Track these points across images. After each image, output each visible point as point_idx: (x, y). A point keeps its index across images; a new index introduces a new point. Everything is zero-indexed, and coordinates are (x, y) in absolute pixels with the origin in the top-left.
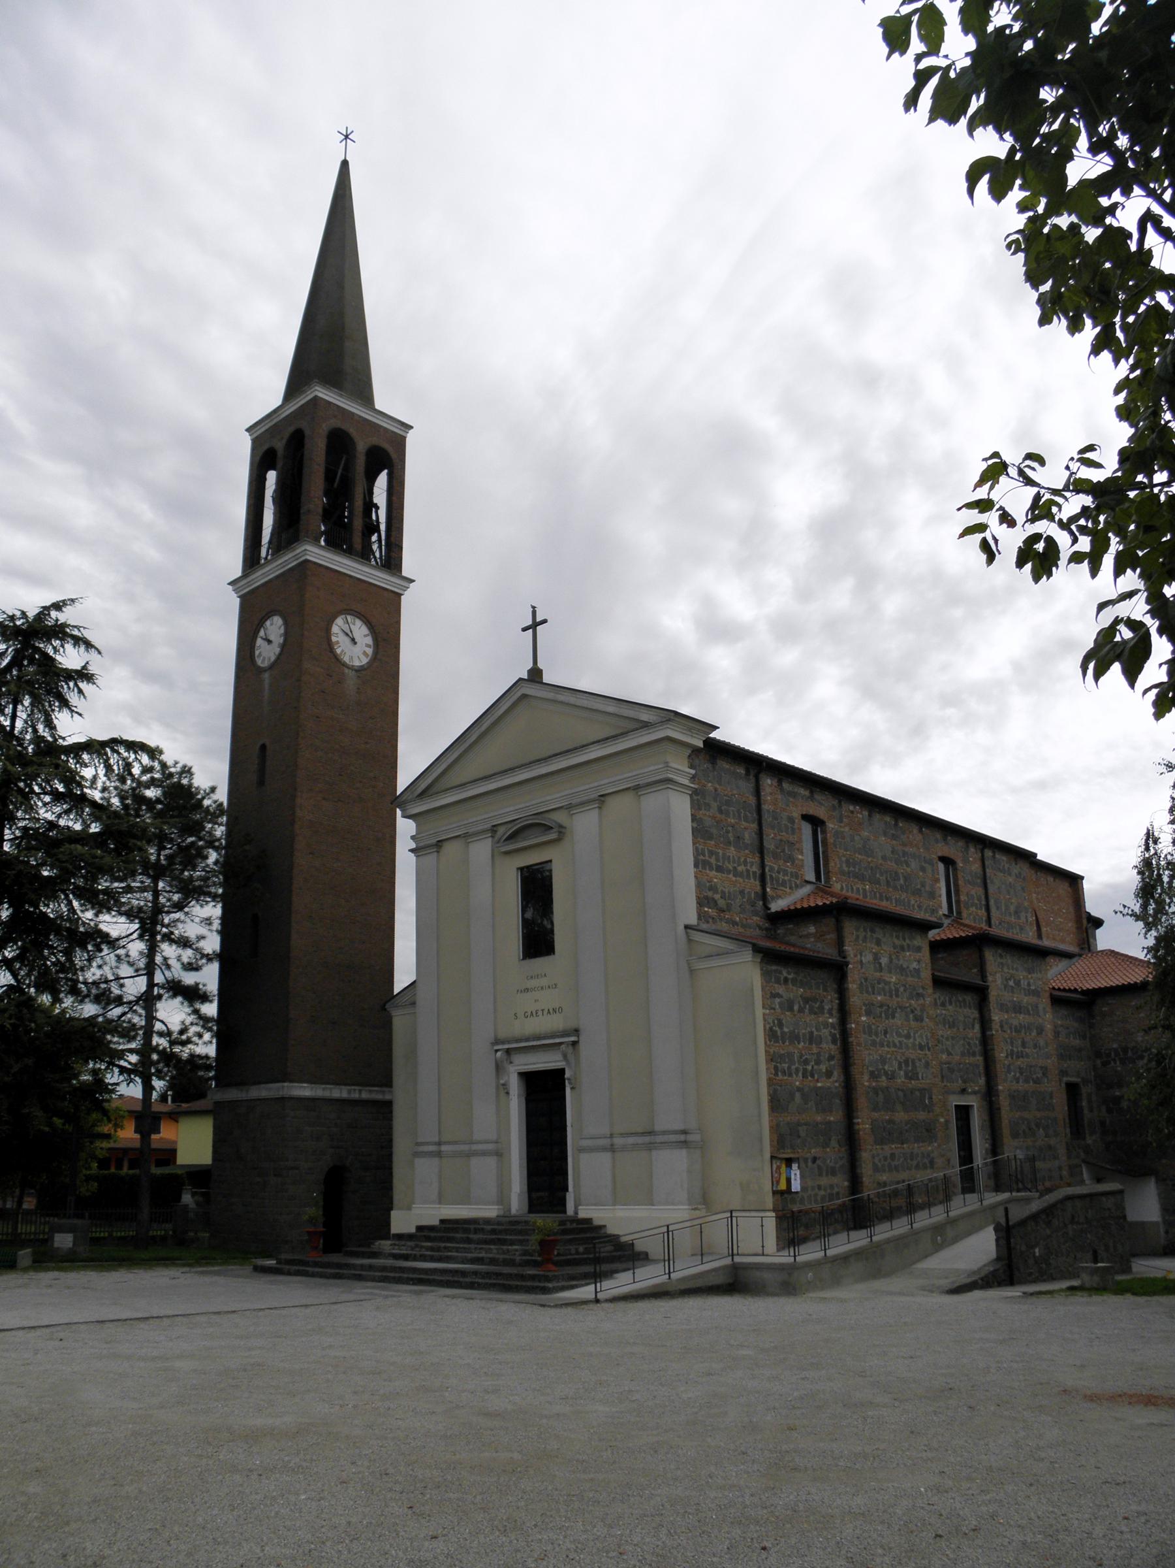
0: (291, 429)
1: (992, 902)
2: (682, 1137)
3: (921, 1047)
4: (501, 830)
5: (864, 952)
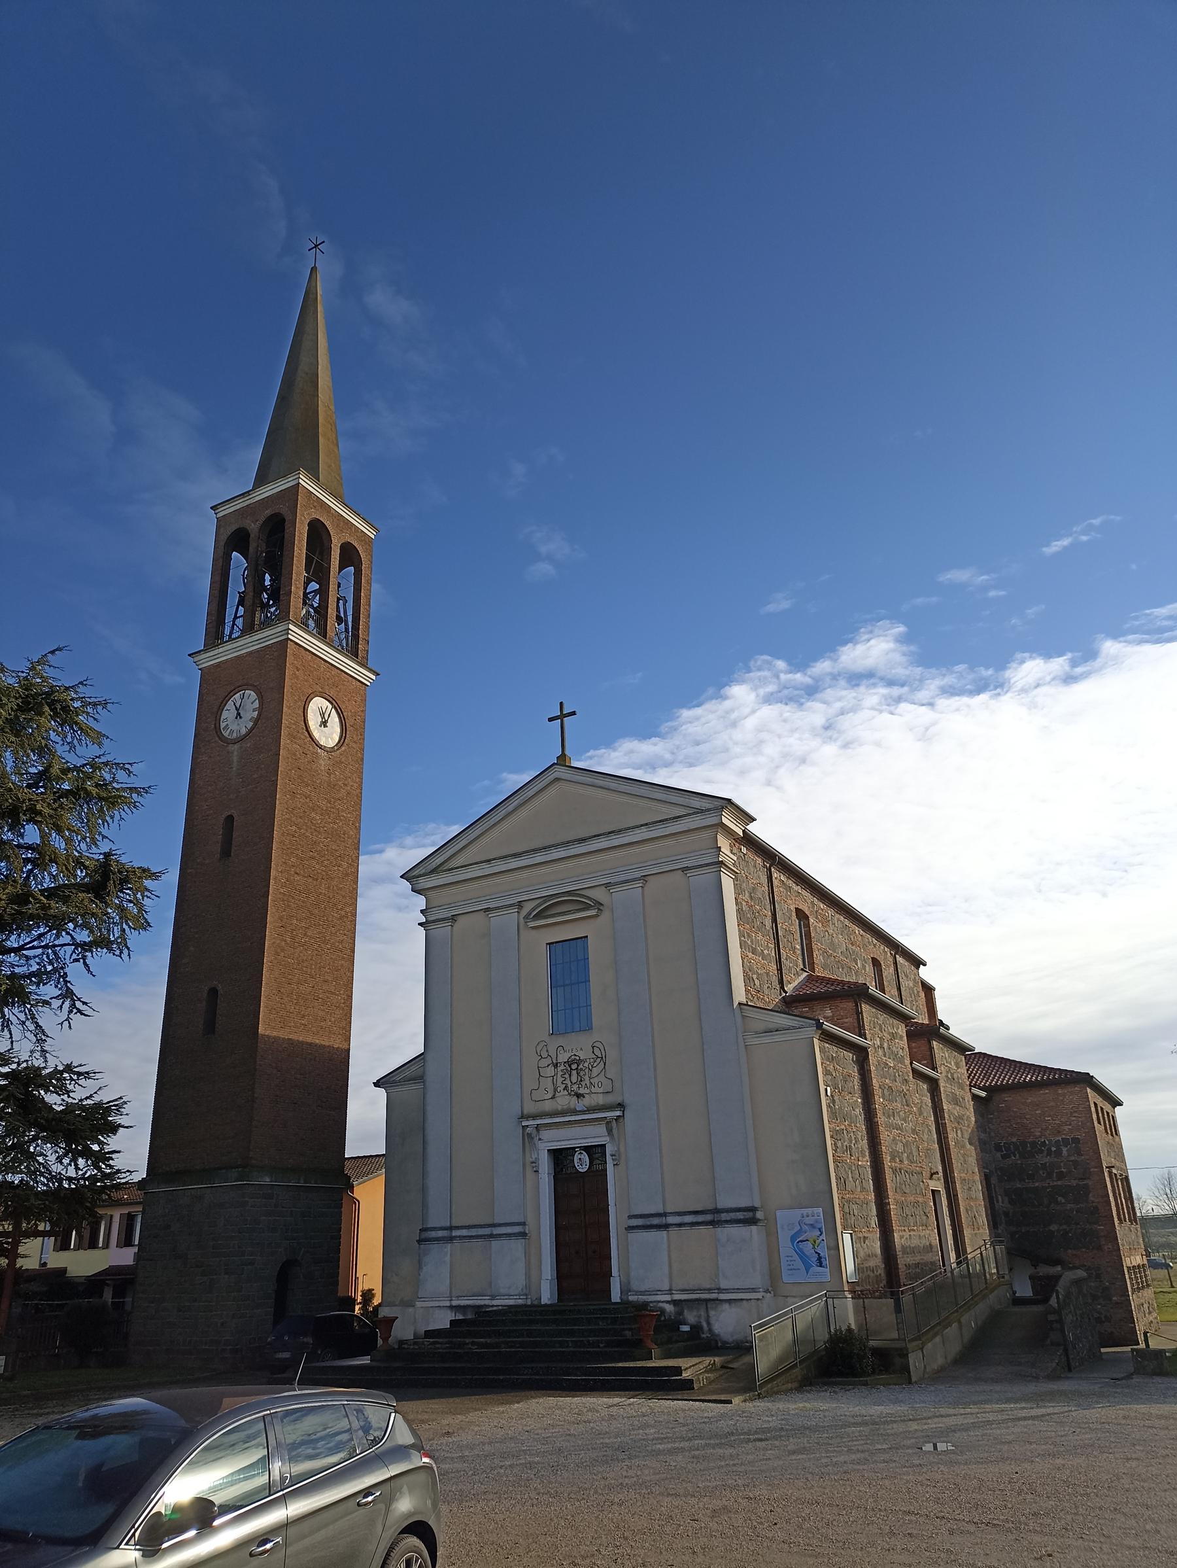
0: (268, 512)
2: (750, 1214)
4: (528, 907)
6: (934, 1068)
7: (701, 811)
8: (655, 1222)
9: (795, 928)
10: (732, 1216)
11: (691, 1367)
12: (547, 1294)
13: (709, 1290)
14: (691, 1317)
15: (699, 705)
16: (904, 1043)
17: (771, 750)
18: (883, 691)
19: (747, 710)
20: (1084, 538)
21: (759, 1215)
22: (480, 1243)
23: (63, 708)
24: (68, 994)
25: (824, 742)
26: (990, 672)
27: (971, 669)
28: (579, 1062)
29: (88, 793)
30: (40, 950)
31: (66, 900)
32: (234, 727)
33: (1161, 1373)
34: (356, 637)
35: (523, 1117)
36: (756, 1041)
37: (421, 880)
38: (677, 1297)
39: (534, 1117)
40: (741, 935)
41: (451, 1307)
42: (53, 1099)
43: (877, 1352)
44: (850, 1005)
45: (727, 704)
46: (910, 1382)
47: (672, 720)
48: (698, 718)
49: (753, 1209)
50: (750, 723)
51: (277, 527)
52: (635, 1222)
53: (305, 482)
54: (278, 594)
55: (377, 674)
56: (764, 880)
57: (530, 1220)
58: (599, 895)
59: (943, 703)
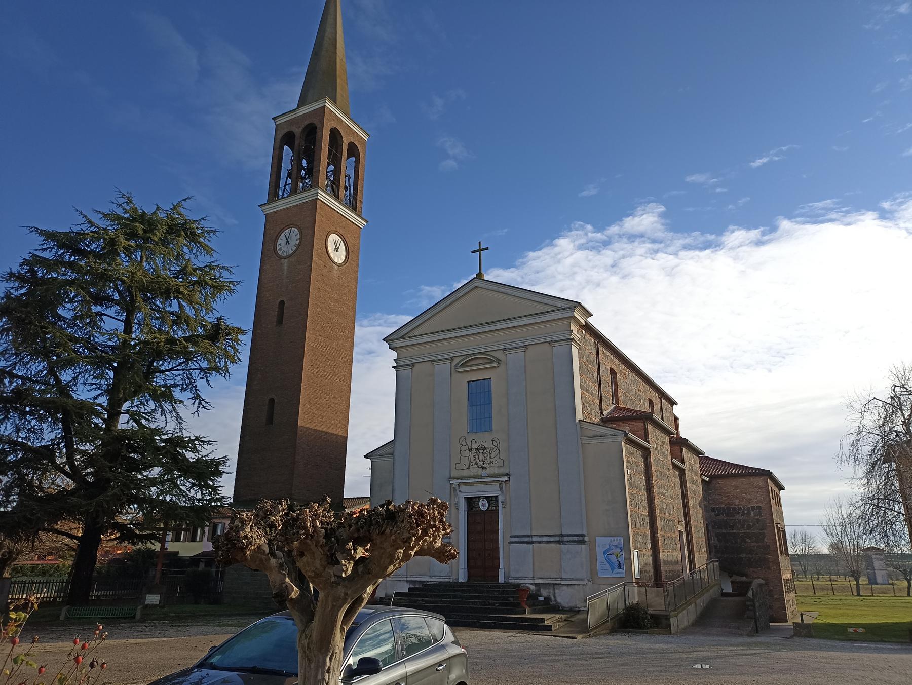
0: (306, 123)
2: (581, 538)
4: (456, 361)
6: (683, 463)
7: (562, 309)
9: (609, 379)
10: (571, 538)
11: (549, 619)
12: (462, 578)
14: (544, 592)
15: (540, 250)
16: (668, 448)
17: (579, 278)
18: (649, 246)
19: (567, 254)
20: (776, 158)
21: (586, 539)
23: (191, 233)
24: (197, 397)
25: (612, 275)
26: (713, 237)
27: (702, 234)
29: (207, 284)
30: (181, 372)
31: (195, 344)
32: (285, 249)
33: (809, 636)
34: (355, 199)
36: (589, 442)
38: (537, 582)
39: (457, 479)
40: (581, 381)
41: (407, 581)
42: (191, 456)
43: (652, 616)
44: (641, 424)
45: (557, 250)
46: (671, 634)
48: (539, 258)
49: (583, 536)
50: (569, 261)
51: (312, 131)
52: (514, 539)
53: (329, 105)
54: (311, 172)
55: (367, 222)
56: (594, 351)
58: (500, 355)
59: (683, 254)
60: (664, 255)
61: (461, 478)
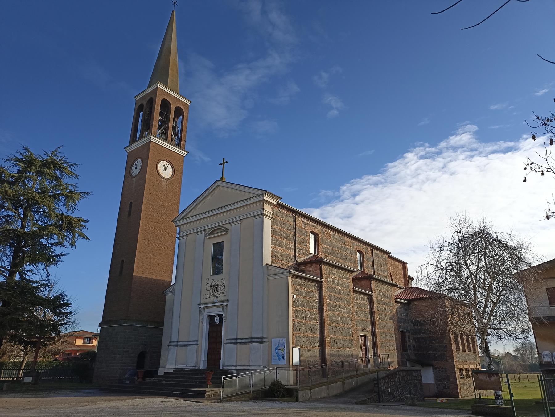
0: (149, 98)
1: (375, 268)
3: (349, 313)
5: (329, 277)
6: (371, 291)
8: (234, 342)
10: (256, 340)
12: (202, 365)
13: (247, 366)
17: (422, 177)
22: (184, 347)
28: (218, 285)
32: (135, 172)
35: (200, 304)
37: (177, 222)
38: (238, 368)
45: (407, 160)
47: (384, 167)
48: (395, 166)
49: (263, 338)
53: (160, 86)
55: (188, 152)
57: (200, 340)
58: (227, 226)
59: (491, 156)
60: (478, 158)
61: (207, 304)
